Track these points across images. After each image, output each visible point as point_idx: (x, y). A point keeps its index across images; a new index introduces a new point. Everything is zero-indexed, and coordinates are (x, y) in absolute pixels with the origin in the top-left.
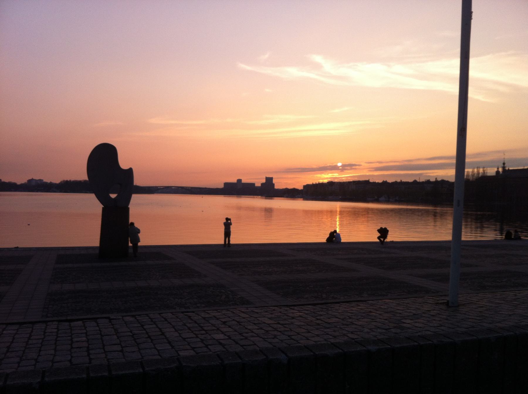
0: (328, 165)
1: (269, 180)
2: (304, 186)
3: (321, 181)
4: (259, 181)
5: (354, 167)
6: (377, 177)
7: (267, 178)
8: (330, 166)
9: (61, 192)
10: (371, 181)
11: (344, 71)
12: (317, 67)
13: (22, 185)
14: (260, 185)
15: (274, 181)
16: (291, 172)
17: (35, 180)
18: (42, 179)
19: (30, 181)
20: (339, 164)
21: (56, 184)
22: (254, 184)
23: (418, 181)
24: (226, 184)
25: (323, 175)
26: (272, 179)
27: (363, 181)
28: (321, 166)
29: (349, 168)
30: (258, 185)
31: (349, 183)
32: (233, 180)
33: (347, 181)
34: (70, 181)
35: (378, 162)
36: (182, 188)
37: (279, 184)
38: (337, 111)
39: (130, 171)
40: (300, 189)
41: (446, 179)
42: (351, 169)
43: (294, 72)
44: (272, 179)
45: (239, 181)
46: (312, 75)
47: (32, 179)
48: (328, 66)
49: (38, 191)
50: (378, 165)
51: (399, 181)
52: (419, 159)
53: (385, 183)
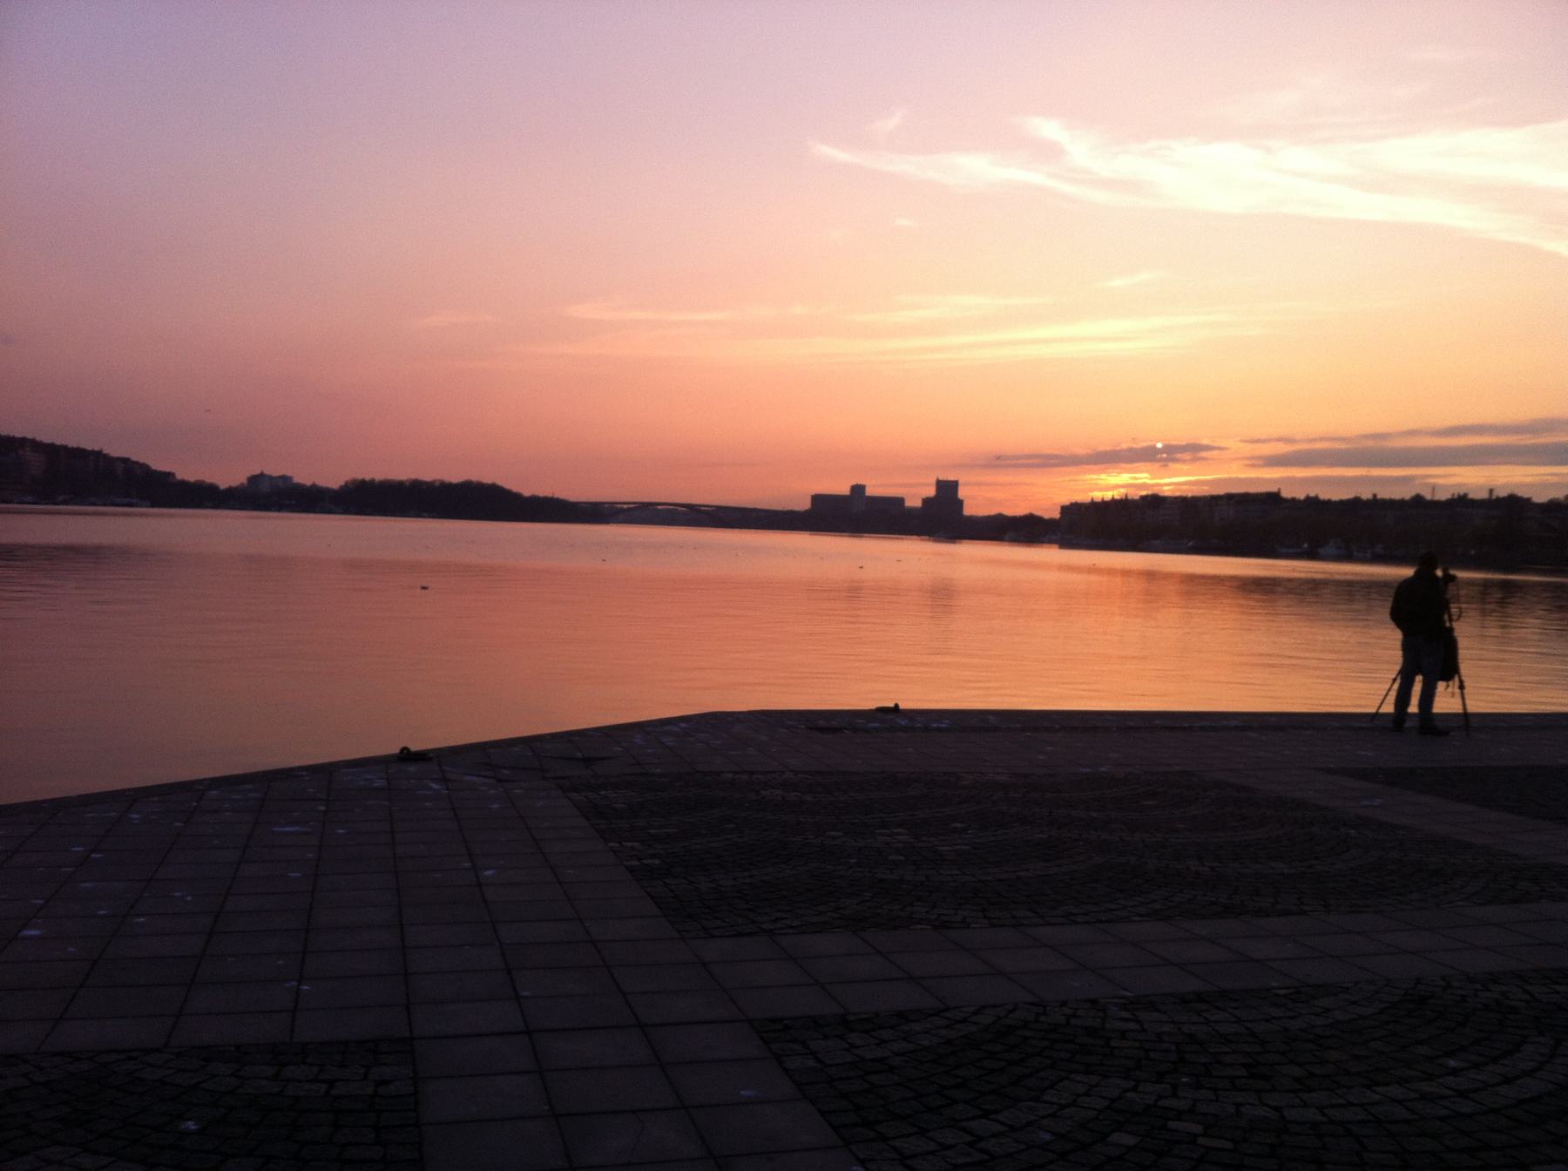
0: (1124, 446)
1: (947, 490)
3: (1098, 495)
4: (916, 492)
5: (1204, 454)
6: (1294, 482)
8: (1130, 450)
9: (346, 512)
10: (1286, 494)
12: (1048, 152)
13: (230, 490)
14: (918, 504)
15: (962, 493)
16: (1015, 466)
17: (271, 477)
18: (289, 474)
19: (254, 480)
20: (1159, 445)
21: (328, 491)
22: (901, 501)
23: (1428, 497)
24: (818, 499)
25: (1103, 476)
26: (953, 486)
27: (1262, 494)
28: (1101, 448)
29: (1187, 456)
30: (914, 502)
31: (1215, 499)
33: (1177, 494)
34: (372, 481)
35: (1279, 440)
36: (691, 507)
37: (977, 501)
38: (1117, 282)
40: (1046, 516)
41: (1037, 513)
42: (1195, 460)
43: (978, 168)
44: (953, 486)
45: (858, 490)
46: (1037, 178)
47: (262, 475)
48: (1081, 149)
49: (280, 507)
50: (1282, 448)
51: (1366, 495)
52: (1412, 433)
53: (1313, 503)
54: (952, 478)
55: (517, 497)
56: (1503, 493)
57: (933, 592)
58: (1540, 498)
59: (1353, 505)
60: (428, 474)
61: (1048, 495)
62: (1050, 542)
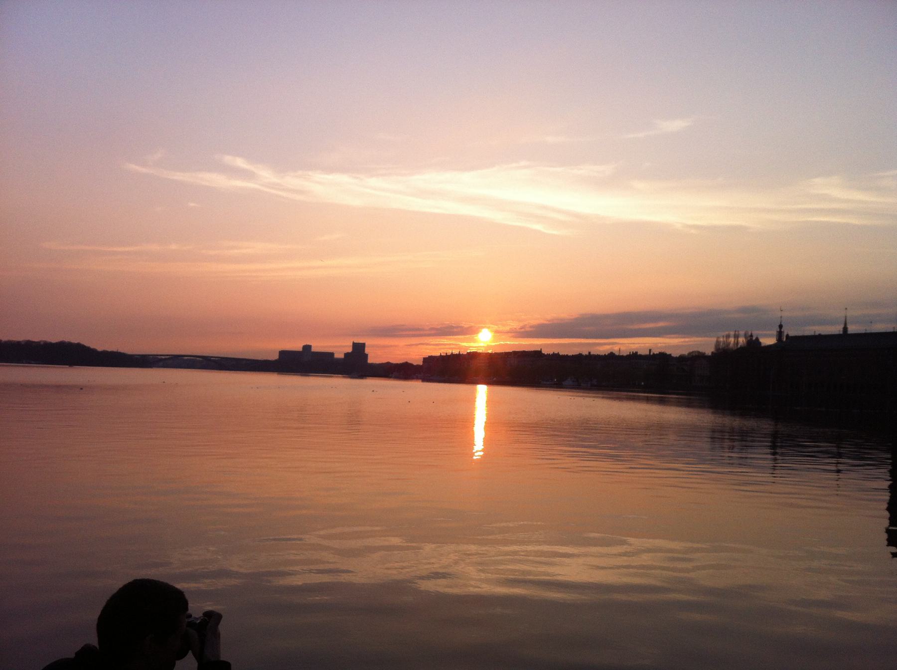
1: (359, 348)
2: (424, 359)
4: (341, 347)
6: (547, 345)
7: (355, 345)
11: (291, 181)
14: (342, 356)
15: (367, 351)
22: (332, 354)
23: (617, 354)
24: (283, 353)
30: (339, 355)
31: (507, 354)
32: (296, 346)
36: (29, 345)
37: (375, 357)
39: (212, 618)
43: (133, 167)
44: (363, 346)
45: (307, 348)
51: (585, 353)
53: (556, 356)
54: (361, 342)
55: (94, 351)
56: (656, 352)
57: (714, 431)
58: (675, 354)
59: (579, 357)
60: (37, 337)
61: (416, 351)
62: (417, 378)
